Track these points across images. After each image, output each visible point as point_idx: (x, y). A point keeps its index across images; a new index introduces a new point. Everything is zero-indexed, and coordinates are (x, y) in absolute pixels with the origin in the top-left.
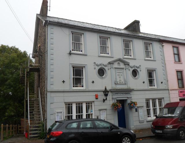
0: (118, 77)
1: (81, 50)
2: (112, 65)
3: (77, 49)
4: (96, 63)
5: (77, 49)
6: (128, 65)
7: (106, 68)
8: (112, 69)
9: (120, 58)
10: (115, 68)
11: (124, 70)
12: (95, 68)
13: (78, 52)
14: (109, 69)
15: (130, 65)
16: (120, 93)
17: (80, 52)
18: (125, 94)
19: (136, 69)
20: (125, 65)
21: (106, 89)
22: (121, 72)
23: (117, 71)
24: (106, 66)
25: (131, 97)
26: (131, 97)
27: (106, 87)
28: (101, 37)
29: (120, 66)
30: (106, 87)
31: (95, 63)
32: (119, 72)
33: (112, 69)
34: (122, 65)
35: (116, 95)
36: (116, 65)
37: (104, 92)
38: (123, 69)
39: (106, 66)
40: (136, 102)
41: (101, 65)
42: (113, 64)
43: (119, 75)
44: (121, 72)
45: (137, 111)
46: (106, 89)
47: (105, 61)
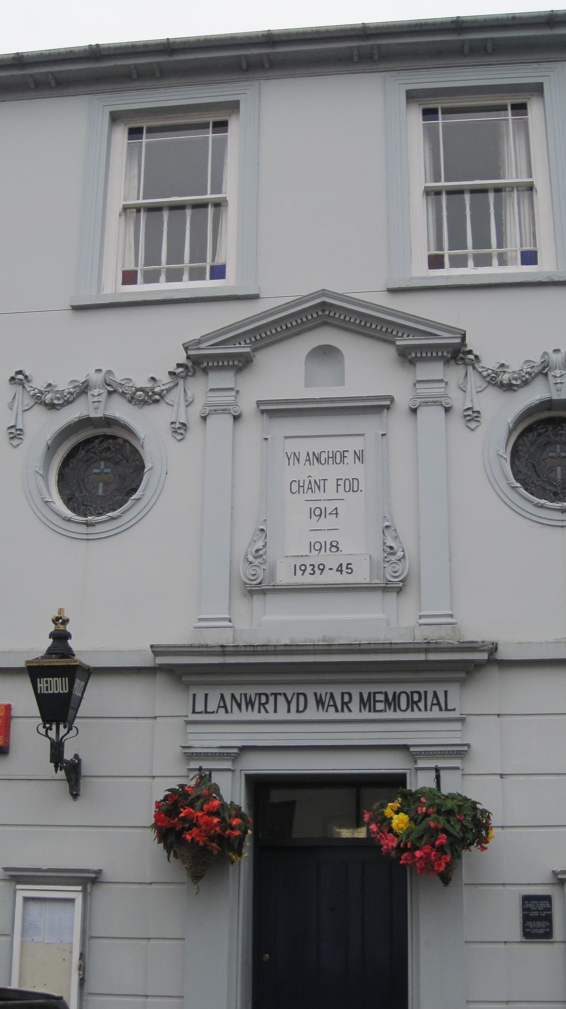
0: (297, 507)
1: (219, 261)
2: (219, 379)
3: (175, 255)
4: (38, 383)
5: (175, 255)
6: (457, 353)
7: (149, 428)
8: (431, 416)
9: (323, 293)
10: (273, 411)
11: (397, 422)
12: (16, 434)
13: (186, 286)
14: (180, 429)
15: (489, 362)
16: (290, 691)
17: (208, 286)
18: (367, 703)
19: (119, 410)
20: (408, 357)
21: (60, 637)
22: (355, 444)
23: (293, 446)
24: (148, 398)
25: (461, 752)
26: (461, 752)
27: (60, 620)
28: (145, 124)
29: (341, 382)
30: (60, 620)
31: (19, 379)
32: (315, 446)
33: (431, 416)
34: (367, 370)
35: (236, 715)
36: (283, 373)
37: (35, 672)
38: (379, 407)
39: (148, 398)
40: (490, 813)
41: (84, 389)
42: (242, 364)
43: (317, 485)
44: (355, 444)
45: (547, 935)
46: (60, 637)
47: (145, 349)
